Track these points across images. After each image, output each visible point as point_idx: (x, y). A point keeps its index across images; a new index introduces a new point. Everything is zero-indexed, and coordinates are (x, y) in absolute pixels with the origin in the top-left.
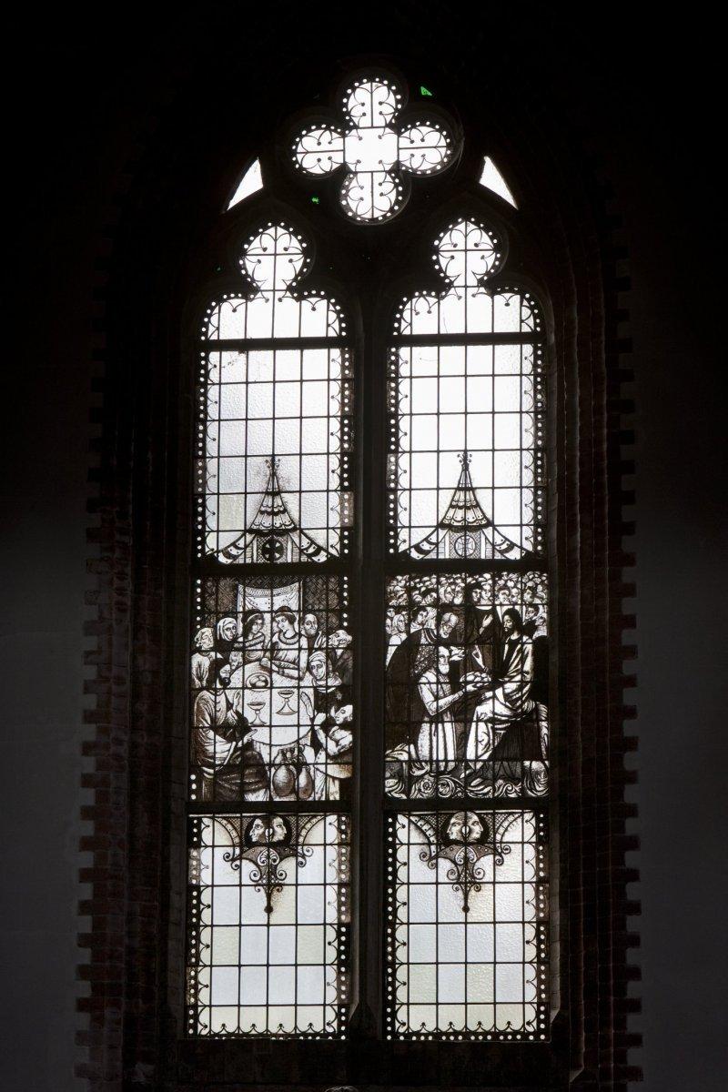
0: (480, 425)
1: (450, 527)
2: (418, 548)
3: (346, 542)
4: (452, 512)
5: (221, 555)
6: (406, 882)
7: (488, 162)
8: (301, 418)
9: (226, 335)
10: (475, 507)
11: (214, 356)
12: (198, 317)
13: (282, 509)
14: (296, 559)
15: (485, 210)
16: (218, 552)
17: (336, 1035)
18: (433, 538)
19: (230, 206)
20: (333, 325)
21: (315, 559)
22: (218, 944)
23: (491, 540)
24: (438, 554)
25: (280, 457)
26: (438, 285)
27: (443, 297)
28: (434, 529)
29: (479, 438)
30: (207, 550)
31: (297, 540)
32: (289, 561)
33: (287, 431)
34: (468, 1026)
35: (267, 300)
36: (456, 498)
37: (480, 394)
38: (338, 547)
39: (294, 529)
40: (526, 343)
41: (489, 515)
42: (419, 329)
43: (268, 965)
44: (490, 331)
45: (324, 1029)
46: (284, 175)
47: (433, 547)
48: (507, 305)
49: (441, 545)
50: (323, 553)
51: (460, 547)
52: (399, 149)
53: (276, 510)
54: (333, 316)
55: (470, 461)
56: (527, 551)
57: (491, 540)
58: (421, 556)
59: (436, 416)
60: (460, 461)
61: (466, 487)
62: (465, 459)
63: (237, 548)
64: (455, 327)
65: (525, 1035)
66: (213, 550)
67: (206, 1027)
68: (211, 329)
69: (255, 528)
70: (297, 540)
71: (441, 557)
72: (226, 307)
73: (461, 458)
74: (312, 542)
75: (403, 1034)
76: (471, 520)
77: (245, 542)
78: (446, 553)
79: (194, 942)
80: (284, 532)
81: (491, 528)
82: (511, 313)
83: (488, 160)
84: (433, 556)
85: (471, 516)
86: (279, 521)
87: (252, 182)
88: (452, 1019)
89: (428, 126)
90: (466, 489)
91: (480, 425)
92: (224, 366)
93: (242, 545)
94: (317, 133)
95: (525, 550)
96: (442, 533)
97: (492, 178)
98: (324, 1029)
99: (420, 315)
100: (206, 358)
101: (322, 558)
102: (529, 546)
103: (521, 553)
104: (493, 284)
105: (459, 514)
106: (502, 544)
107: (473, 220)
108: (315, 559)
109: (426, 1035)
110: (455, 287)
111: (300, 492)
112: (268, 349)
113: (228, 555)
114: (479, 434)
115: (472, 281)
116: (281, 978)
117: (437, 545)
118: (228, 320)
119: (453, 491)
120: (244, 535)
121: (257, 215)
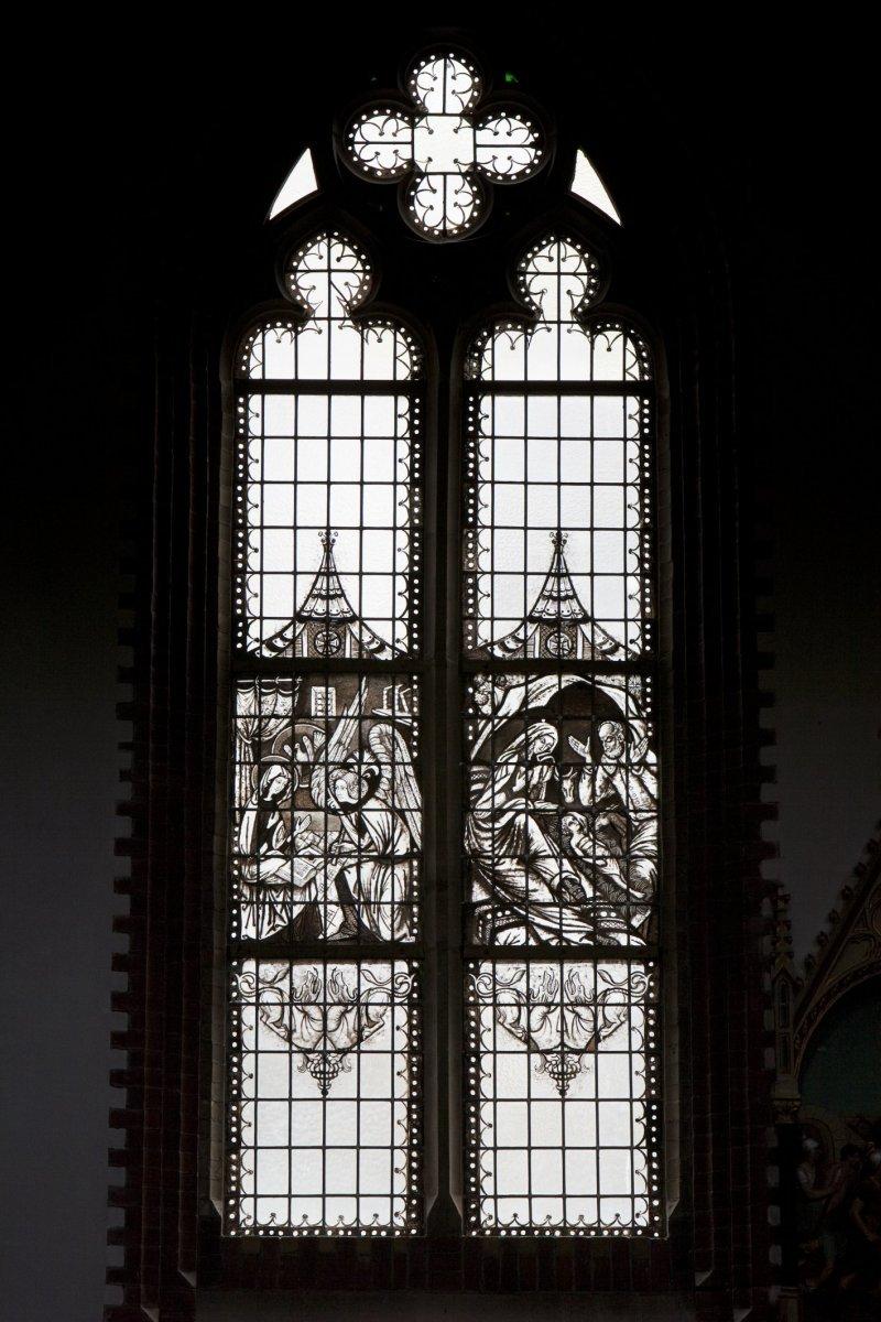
0: (344, 500)
1: (538, 620)
2: (502, 644)
3: (415, 636)
4: (311, 603)
5: (496, 647)
6: (491, 1049)
7: (582, 163)
8: (329, 483)
9: (503, 375)
10: (340, 596)
11: (486, 402)
12: (237, 348)
13: (339, 593)
14: (588, 656)
15: (578, 223)
16: (492, 644)
17: (647, 1230)
18: (289, 634)
19: (273, 214)
20: (257, 363)
21: (379, 656)
22: (263, 1123)
23: (358, 637)
24: (526, 652)
25: (568, 532)
26: (526, 318)
27: (531, 334)
28: (289, 621)
29: (575, 515)
30: (479, 641)
31: (589, 635)
32: (347, 656)
33: (344, 500)
34: (361, 1219)
35: (320, 332)
36: (318, 586)
37: (345, 460)
38: (406, 641)
39: (353, 619)
40: (630, 395)
41: (587, 608)
42: (279, 370)
43: (290, 1148)
44: (357, 377)
45: (392, 1222)
46: (338, 171)
47: (520, 645)
48: (279, 341)
49: (529, 642)
50: (622, 650)
51: (552, 645)
52: (412, 143)
53: (563, 594)
54: (401, 349)
55: (565, 541)
56: (635, 653)
57: (358, 637)
58: (274, 654)
59: (332, 486)
60: (322, 541)
61: (328, 572)
62: (559, 535)
63: (284, 639)
64: (313, 371)
65: (634, 1229)
66: (486, 641)
67: (249, 1217)
68: (253, 362)
69: (537, 615)
70: (589, 635)
71: (530, 656)
72: (271, 335)
73: (324, 537)
74: (375, 636)
75: (489, 1228)
76: (566, 613)
77: (526, 628)
78: (535, 652)
79: (234, 1119)
80: (344, 621)
81: (358, 623)
82: (614, 357)
83: (307, 154)
84: (520, 656)
85: (565, 608)
86: (566, 608)
87: (301, 181)
88: (546, 1214)
89: (492, 120)
90: (559, 576)
91: (576, 499)
92: (270, 415)
93: (522, 637)
94: (379, 120)
95: (398, 650)
96: (531, 628)
97: (587, 184)
98: (392, 1222)
99: (504, 356)
100: (477, 404)
101: (386, 655)
102: (402, 647)
103: (393, 653)
104: (362, 315)
105: (320, 606)
106: (604, 643)
107: (569, 240)
108: (379, 656)
109: (276, 1229)
110: (315, 319)
111: (592, 574)
112: (289, 393)
113: (272, 647)
114: (345, 509)
115: (566, 315)
116: (580, 1163)
117: (293, 642)
118: (273, 353)
119: (544, 577)
120: (293, 623)
121: (310, 221)
